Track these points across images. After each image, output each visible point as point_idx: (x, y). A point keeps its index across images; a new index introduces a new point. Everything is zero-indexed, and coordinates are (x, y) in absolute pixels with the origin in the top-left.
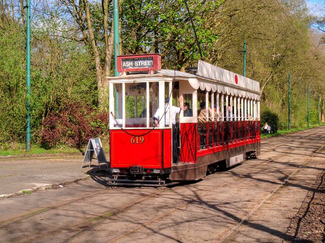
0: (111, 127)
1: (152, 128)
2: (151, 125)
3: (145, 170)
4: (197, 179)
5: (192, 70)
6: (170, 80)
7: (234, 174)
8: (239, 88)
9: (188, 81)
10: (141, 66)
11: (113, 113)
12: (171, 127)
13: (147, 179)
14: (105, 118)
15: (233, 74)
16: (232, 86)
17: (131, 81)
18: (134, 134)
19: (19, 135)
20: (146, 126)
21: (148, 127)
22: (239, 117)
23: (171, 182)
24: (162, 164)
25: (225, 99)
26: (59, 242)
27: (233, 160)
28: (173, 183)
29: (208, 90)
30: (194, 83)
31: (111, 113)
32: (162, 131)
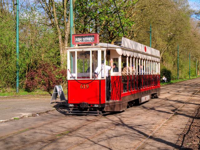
0: (69, 78)
1: (94, 79)
2: (93, 77)
3: (90, 105)
4: (121, 111)
5: (118, 43)
6: (105, 49)
7: (144, 107)
8: (147, 55)
9: (115, 50)
10: (87, 41)
11: (70, 70)
12: (105, 78)
13: (90, 110)
14: (64, 73)
15: (143, 46)
16: (143, 53)
17: (81, 50)
18: (83, 83)
19: (12, 83)
20: (90, 78)
21: (91, 79)
22: (147, 72)
23: (106, 112)
24: (100, 101)
25: (138, 61)
27: (143, 99)
28: (107, 113)
29: (128, 55)
30: (119, 51)
31: (69, 70)
32: (100, 81)
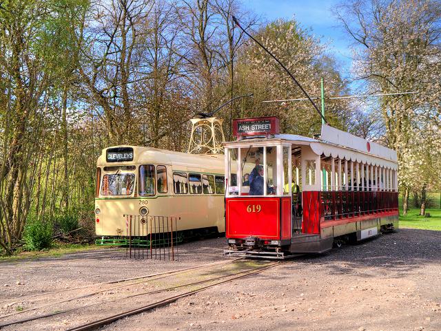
6: (289, 145)
12: (290, 195)
17: (247, 146)
18: (251, 202)
20: (262, 194)
22: (363, 186)
25: (378, 171)
26: (147, 329)
29: (334, 156)
32: (280, 199)
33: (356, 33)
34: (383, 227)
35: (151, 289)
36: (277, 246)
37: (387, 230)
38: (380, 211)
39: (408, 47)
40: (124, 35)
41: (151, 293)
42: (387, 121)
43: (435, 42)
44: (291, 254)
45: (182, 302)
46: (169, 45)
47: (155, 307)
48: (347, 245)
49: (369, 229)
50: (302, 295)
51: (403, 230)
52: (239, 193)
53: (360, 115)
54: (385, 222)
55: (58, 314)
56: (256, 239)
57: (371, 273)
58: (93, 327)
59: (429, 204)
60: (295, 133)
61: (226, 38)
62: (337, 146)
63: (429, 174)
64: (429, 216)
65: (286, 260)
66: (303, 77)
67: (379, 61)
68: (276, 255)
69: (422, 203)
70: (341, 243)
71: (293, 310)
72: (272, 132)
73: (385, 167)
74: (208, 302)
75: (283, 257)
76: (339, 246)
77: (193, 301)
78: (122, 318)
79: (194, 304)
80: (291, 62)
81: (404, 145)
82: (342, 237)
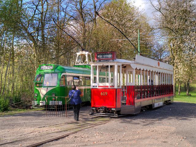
6: (120, 64)
17: (101, 64)
33: (156, 6)
34: (166, 101)
35: (57, 131)
36: (114, 111)
37: (167, 103)
38: (164, 94)
39: (181, 13)
40: (42, 5)
41: (57, 132)
42: (171, 49)
43: (194, 11)
44: (121, 115)
45: (71, 136)
46: (65, 11)
47: (59, 138)
48: (148, 111)
49: (158, 102)
50: (124, 133)
51: (175, 103)
52: (98, 86)
53: (158, 45)
54: (166, 99)
55: (16, 141)
56: (105, 108)
57: (138, 122)
58: (37, 146)
59: (191, 89)
60: (124, 59)
61: (93, 7)
62: (143, 65)
63: (190, 75)
64: (190, 95)
65: (118, 117)
66: (130, 28)
67: (167, 20)
68: (114, 115)
69: (188, 89)
70: (145, 109)
71: (120, 140)
72: (113, 59)
73: (169, 74)
74: (83, 136)
75: (117, 116)
76: (144, 111)
77: (76, 136)
78: (45, 143)
79: (76, 137)
80: (124, 20)
81: (178, 61)
82: (145, 107)
